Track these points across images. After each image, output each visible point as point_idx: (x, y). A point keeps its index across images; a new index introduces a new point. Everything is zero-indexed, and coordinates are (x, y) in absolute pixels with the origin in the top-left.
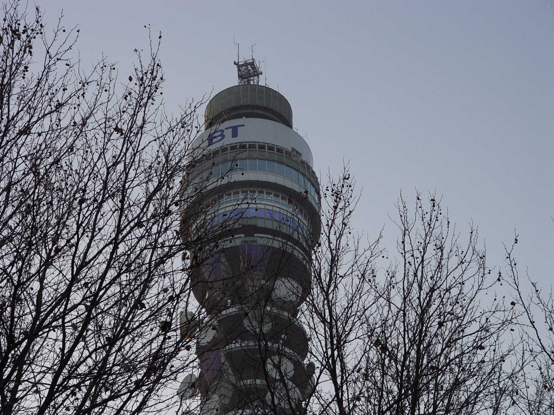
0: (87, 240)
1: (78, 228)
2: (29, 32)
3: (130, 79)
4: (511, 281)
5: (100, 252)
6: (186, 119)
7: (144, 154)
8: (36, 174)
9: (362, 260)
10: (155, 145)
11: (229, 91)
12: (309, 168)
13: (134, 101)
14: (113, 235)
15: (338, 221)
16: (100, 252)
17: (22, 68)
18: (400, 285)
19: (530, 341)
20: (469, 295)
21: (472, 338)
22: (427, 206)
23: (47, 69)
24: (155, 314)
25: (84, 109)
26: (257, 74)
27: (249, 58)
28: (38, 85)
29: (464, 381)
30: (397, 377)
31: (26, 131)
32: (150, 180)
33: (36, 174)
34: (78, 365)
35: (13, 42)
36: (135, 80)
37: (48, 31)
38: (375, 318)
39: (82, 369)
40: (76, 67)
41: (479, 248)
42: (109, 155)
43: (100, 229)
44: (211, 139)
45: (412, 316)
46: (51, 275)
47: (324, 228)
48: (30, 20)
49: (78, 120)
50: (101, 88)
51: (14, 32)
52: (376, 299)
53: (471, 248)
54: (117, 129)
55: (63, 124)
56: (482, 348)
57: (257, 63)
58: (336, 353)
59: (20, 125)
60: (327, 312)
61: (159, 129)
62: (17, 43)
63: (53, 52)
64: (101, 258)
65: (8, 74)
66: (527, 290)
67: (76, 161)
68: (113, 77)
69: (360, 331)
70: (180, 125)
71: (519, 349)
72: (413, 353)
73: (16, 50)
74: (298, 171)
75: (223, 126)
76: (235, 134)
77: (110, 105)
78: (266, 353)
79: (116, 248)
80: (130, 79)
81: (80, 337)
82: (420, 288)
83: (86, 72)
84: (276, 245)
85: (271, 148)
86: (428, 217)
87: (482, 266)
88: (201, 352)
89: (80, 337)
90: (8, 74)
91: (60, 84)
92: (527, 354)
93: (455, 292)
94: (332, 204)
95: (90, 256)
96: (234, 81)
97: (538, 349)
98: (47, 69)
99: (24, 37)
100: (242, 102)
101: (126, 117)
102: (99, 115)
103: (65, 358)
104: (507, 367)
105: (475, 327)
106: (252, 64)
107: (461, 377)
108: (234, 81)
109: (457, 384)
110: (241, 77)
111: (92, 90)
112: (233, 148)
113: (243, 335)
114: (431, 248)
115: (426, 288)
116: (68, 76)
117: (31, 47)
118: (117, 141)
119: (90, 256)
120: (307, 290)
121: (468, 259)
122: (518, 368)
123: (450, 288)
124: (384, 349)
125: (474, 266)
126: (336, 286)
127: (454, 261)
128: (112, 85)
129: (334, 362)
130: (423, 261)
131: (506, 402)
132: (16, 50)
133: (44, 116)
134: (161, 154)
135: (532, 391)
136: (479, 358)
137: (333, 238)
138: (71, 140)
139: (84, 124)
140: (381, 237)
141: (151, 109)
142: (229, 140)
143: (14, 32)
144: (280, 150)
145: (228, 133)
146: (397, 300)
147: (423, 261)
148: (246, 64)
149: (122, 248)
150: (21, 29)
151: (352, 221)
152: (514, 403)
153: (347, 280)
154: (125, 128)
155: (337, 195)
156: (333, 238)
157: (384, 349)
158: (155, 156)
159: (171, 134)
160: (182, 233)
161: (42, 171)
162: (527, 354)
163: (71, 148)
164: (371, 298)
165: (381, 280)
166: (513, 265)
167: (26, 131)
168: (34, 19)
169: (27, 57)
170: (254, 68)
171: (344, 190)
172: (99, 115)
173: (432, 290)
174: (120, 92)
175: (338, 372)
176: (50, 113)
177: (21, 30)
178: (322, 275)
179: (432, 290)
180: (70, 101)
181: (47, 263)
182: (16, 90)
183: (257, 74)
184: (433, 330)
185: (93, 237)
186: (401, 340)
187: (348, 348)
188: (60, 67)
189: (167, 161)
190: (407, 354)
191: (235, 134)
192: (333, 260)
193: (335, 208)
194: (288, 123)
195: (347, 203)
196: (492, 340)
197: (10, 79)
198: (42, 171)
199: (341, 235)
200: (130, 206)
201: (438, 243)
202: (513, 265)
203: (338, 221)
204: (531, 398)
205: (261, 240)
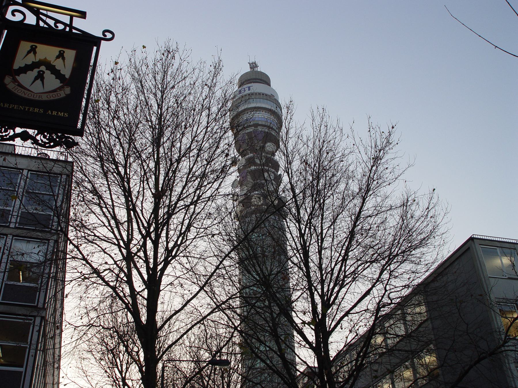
0: (196, 127)
1: (193, 122)
2: (174, 51)
3: (211, 66)
4: (352, 137)
5: (202, 131)
6: (232, 80)
7: (216, 94)
8: (177, 103)
9: (298, 131)
10: (220, 91)
11: (247, 73)
12: (278, 101)
13: (213, 75)
14: (206, 125)
15: (289, 117)
16: (202, 131)
17: (171, 65)
18: (312, 140)
19: (359, 159)
20: (337, 143)
21: (338, 159)
22: (321, 111)
23: (180, 65)
24: (223, 152)
25: (194, 78)
26: (257, 67)
27: (254, 61)
28: (177, 71)
29: (336, 174)
30: (312, 175)
31: (173, 87)
32: (219, 104)
33: (177, 103)
34: (195, 172)
35: (168, 55)
36: (212, 67)
37: (181, 51)
38: (303, 153)
39: (197, 174)
40: (190, 63)
41: (341, 126)
42: (204, 95)
43: (201, 123)
44: (240, 92)
45: (317, 152)
46: (184, 140)
47: (284, 121)
48: (174, 47)
49: (192, 83)
50: (200, 71)
51: (169, 51)
52: (303, 146)
53: (337, 126)
54: (206, 85)
55: (187, 85)
56: (342, 161)
57: (257, 63)
58: (289, 166)
59: (171, 86)
60: (285, 151)
61: (222, 84)
62: (169, 55)
63: (182, 58)
64: (202, 133)
65: (166, 67)
66: (358, 140)
67: (192, 98)
68: (205, 66)
69: (297, 157)
70: (230, 83)
71: (355, 162)
72: (317, 165)
73: (169, 58)
74: (273, 102)
75: (245, 86)
76: (249, 90)
77: (204, 77)
78: (263, 171)
79: (207, 129)
80: (211, 66)
81: (196, 161)
82: (319, 141)
83: (195, 65)
84: (267, 130)
85: (263, 94)
86: (321, 115)
87: (342, 132)
88: (239, 170)
89: (196, 161)
90: (166, 67)
91: (185, 70)
92: (358, 163)
93: (332, 142)
94: (286, 111)
95: (198, 133)
96: (249, 70)
97: (361, 161)
98: (180, 65)
99: (172, 53)
100: (252, 77)
101: (210, 81)
102: (200, 81)
103: (191, 170)
104: (351, 168)
105: (340, 154)
106: (255, 63)
107: (335, 173)
108: (249, 70)
109: (333, 175)
110: (251, 68)
111: (197, 71)
112: (249, 95)
113: (255, 164)
114: (323, 126)
115: (321, 141)
116: (188, 67)
117: (174, 57)
118: (206, 89)
119: (198, 133)
120: (278, 147)
121: (336, 130)
122: (355, 169)
123: (330, 141)
124: (306, 163)
125: (339, 133)
126: (288, 142)
127: (331, 131)
128: (204, 69)
129: (288, 169)
130: (320, 130)
131: (350, 181)
132: (169, 58)
133: (180, 82)
134: (223, 94)
135: (360, 176)
136: (341, 165)
137: (287, 124)
138: (189, 90)
139: (194, 84)
140: (305, 123)
141: (218, 77)
142: (247, 92)
143: (169, 51)
144: (266, 95)
145: (247, 89)
146: (311, 145)
147: (320, 130)
148: (252, 63)
149: (209, 129)
150: (171, 51)
151: (294, 118)
152: (353, 180)
153: (293, 139)
154: (209, 84)
155: (288, 108)
156: (287, 124)
157: (306, 163)
158: (220, 95)
159: (191, 353)
160: (231, 123)
161: (179, 102)
162: (358, 163)
163: (190, 93)
164: (302, 145)
165: (305, 139)
166: (353, 131)
167: (173, 87)
168: (176, 47)
169: (173, 60)
170: (256, 65)
171: (291, 106)
172: (200, 81)
173: (324, 142)
174: (207, 72)
175: (290, 173)
176: (182, 80)
177: (171, 51)
178: (283, 137)
179: (324, 142)
180: (189, 76)
181: (183, 134)
182: (169, 73)
183: (257, 67)
184: (324, 156)
185: (199, 126)
186: (313, 160)
187: (294, 164)
188: (185, 63)
189: (225, 96)
190: (315, 165)
191: (249, 90)
192: (287, 132)
193: (288, 112)
194: (270, 85)
195: (292, 110)
196: (345, 159)
197: (167, 69)
198: (179, 102)
199: (290, 123)
200: (212, 114)
201: (325, 124)
202: (353, 131)
203: (289, 117)
204: (359, 179)
205: (260, 129)
